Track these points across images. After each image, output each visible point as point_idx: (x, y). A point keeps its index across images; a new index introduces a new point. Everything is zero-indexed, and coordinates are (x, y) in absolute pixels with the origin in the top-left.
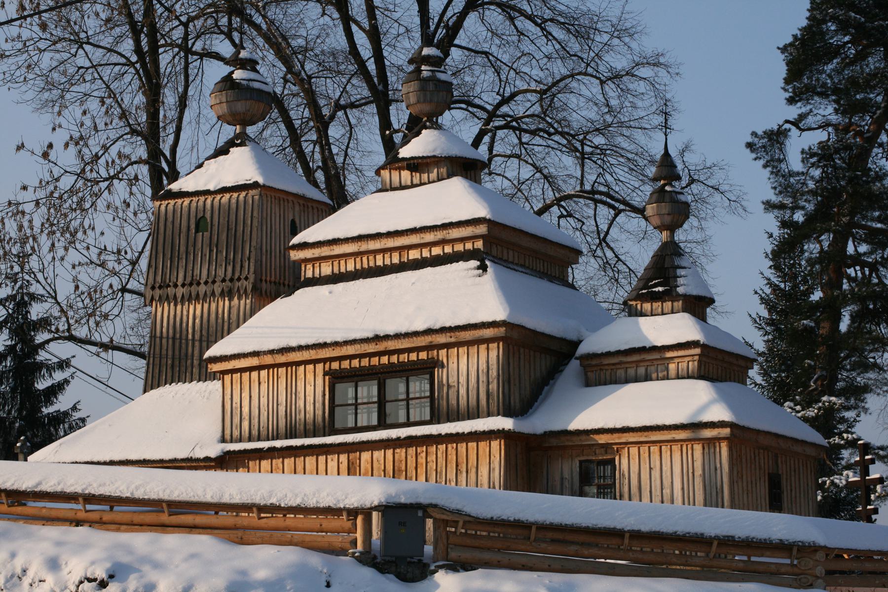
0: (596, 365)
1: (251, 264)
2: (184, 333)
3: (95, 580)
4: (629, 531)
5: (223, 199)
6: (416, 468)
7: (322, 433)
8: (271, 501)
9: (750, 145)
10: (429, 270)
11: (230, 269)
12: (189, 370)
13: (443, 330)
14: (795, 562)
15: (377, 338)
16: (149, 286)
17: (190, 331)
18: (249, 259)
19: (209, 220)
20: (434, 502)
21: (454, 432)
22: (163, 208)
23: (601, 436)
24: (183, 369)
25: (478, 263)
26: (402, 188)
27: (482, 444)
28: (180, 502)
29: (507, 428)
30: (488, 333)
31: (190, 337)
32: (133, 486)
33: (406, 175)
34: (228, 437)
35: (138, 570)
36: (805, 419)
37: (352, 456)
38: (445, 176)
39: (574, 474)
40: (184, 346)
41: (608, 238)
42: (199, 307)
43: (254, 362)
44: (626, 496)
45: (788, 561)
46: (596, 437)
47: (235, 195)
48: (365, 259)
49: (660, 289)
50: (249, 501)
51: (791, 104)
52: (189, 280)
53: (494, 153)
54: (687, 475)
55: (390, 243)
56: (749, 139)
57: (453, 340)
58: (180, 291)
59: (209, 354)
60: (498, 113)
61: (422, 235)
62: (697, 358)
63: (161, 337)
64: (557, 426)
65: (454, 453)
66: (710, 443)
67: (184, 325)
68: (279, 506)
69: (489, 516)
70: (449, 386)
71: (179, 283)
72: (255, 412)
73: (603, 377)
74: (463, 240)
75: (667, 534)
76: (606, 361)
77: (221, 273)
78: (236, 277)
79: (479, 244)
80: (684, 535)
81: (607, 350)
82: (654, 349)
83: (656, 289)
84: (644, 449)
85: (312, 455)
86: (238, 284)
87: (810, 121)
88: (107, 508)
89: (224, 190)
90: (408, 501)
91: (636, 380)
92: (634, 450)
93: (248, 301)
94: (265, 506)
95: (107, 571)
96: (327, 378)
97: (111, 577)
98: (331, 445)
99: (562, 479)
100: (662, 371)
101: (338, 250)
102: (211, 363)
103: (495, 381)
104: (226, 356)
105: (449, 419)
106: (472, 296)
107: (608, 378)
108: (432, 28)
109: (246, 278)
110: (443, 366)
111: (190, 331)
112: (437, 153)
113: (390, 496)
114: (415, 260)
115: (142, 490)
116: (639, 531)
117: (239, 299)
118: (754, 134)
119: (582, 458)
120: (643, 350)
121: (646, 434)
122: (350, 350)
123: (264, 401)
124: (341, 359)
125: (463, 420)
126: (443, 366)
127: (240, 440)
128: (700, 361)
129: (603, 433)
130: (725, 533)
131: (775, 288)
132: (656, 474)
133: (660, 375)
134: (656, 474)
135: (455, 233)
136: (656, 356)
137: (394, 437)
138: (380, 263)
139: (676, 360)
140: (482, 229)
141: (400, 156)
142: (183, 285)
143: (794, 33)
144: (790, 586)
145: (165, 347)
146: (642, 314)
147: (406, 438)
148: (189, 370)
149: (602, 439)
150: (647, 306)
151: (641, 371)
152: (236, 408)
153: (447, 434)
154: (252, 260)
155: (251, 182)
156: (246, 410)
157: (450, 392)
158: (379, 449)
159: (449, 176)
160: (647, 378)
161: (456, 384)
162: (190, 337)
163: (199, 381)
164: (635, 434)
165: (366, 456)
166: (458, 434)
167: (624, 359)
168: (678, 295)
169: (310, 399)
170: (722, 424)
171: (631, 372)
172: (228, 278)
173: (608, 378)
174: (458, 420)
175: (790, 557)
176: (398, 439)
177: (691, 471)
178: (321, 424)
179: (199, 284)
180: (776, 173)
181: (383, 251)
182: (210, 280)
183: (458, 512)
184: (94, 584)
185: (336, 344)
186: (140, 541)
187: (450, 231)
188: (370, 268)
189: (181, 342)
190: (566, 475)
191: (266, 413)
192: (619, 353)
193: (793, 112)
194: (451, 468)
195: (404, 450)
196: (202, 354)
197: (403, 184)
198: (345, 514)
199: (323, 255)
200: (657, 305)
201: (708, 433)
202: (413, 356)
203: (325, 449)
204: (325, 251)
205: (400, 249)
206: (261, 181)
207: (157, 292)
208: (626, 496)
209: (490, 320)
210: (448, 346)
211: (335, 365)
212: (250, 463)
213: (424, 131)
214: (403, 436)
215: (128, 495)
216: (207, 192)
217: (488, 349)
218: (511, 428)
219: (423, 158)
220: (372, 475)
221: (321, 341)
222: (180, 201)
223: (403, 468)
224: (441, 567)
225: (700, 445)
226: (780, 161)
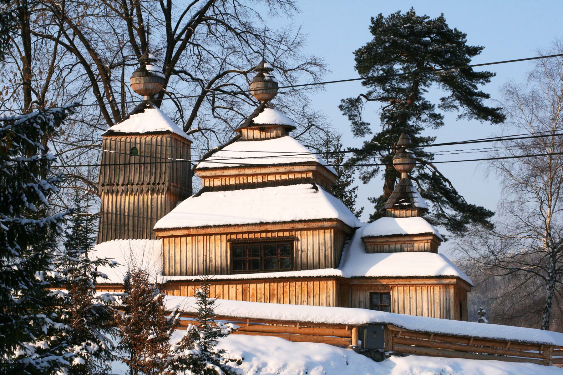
0: (373, 242)
1: (166, 176)
2: (123, 211)
3: (235, 360)
4: (474, 337)
5: (147, 138)
6: (283, 294)
7: (226, 272)
8: (308, 320)
9: (341, 107)
10: (282, 187)
11: (153, 178)
12: (126, 232)
13: (301, 221)
14: (542, 352)
15: (262, 224)
16: (101, 184)
17: (126, 210)
18: (165, 173)
19: (138, 149)
20: (391, 322)
21: (308, 276)
22: (108, 141)
23: (384, 280)
24: (122, 232)
25: (312, 186)
26: (256, 140)
27: (322, 283)
28: (257, 319)
29: (338, 275)
30: (326, 224)
31: (126, 214)
32: (231, 310)
33: (257, 134)
34: (167, 272)
35: (255, 356)
37: (244, 286)
38: (280, 135)
39: (367, 299)
40: (123, 219)
42: (132, 198)
43: (186, 232)
44: (396, 311)
45: (538, 352)
46: (381, 281)
47: (155, 137)
48: (241, 178)
49: (406, 204)
50: (296, 319)
51: (365, 85)
52: (126, 182)
53: (215, 106)
54: (431, 302)
55: (258, 171)
56: (340, 103)
57: (306, 227)
58: (121, 188)
59: (156, 227)
60: (180, 74)
61: (277, 168)
62: (430, 241)
63: (108, 213)
64: (359, 274)
65: (306, 286)
66: (446, 286)
67: (123, 207)
68: (313, 323)
69: (414, 329)
70: (302, 251)
71: (120, 184)
72: (184, 260)
73: (376, 248)
74: (300, 172)
75: (490, 339)
76: (379, 240)
77: (147, 179)
78: (157, 182)
79: (310, 175)
80: (497, 339)
81: (380, 234)
82: (407, 235)
83: (404, 204)
84: (407, 288)
85: (220, 284)
86: (158, 187)
87: (374, 95)
89: (148, 133)
90: (380, 322)
91: (395, 251)
92: (401, 288)
93: (163, 196)
94: (305, 322)
95: (241, 355)
96: (229, 243)
97: (243, 359)
98: (234, 280)
99: (360, 301)
100: (410, 247)
101: (226, 173)
103: (329, 250)
104: (169, 229)
105: (302, 269)
106: (312, 204)
107: (379, 249)
108: (173, 29)
109: (163, 184)
110: (298, 240)
111: (126, 210)
112: (277, 122)
113: (371, 319)
114: (272, 181)
115: (236, 312)
116: (478, 337)
117: (158, 195)
118: (343, 101)
119: (371, 291)
120: (401, 235)
121: (409, 280)
122: (245, 229)
123: (189, 254)
124: (237, 233)
125: (311, 269)
126: (298, 240)
127: (175, 274)
128: (431, 244)
130: (514, 339)
132: (413, 301)
133: (409, 249)
134: (413, 301)
135: (297, 168)
136: (408, 239)
137: (272, 277)
138: (255, 181)
139: (418, 242)
140: (313, 168)
141: (256, 122)
142: (123, 185)
144: (539, 364)
145: (110, 219)
146: (395, 216)
147: (279, 278)
148: (126, 232)
149: (384, 282)
150: (397, 212)
151: (398, 246)
152: (172, 257)
153: (304, 277)
154: (167, 174)
155: (165, 130)
156: (178, 258)
157: (303, 254)
158: (261, 283)
159: (283, 136)
160: (401, 250)
161: (306, 250)
162: (126, 214)
163: (133, 239)
164: (403, 280)
165: (253, 286)
166: (310, 277)
167: (389, 240)
168: (416, 207)
169: (218, 254)
170: (452, 277)
171: (392, 246)
172: (152, 183)
173: (379, 249)
174: (308, 269)
175: (539, 350)
176: (275, 278)
177: (432, 300)
178: (225, 268)
179: (132, 184)
180: (355, 123)
181: (253, 175)
182: (140, 183)
183: (401, 327)
184: (235, 363)
185: (237, 225)
186: (259, 341)
187: (294, 167)
188: (244, 183)
189: (120, 217)
190: (362, 299)
191: (191, 261)
192: (387, 236)
193: (365, 90)
194: (304, 294)
195: (276, 284)
196: (152, 225)
197: (255, 137)
198: (298, 324)
199: (217, 174)
200: (403, 212)
201: (447, 281)
202: (281, 234)
203: (243, 282)
204: (218, 173)
205: (263, 175)
206: (171, 130)
207: (107, 188)
208: (396, 311)
209: (329, 218)
210: (301, 230)
211: (233, 237)
212: (182, 287)
213: (265, 109)
214: (278, 277)
215: (228, 314)
216: (138, 134)
217: (325, 232)
219: (269, 124)
221: (228, 223)
222: (119, 137)
223: (276, 293)
224: (392, 354)
225: (438, 287)
226: (356, 116)
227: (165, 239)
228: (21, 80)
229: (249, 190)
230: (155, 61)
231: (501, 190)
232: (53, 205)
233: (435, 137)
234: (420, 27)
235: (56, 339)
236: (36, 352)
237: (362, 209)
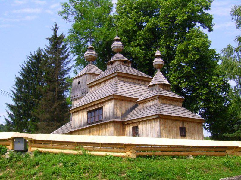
228: (153, 172)
229: (104, 143)
233: (47, 39)
234: (226, 105)
235: (16, 105)
237: (30, 53)
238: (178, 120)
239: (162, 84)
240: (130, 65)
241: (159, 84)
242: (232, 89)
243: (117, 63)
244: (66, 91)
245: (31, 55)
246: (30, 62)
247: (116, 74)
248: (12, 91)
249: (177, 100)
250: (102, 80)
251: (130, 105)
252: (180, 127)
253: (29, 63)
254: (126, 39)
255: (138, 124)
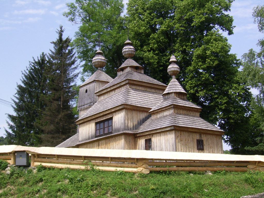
36: (231, 33)
41: (100, 130)
88: (102, 162)
102: (62, 40)
129: (90, 120)
131: (166, 135)
143: (70, 38)
209: (169, 159)
218: (15, 116)
220: (163, 151)
227: (99, 134)
230: (112, 30)
231: (5, 127)
232: (166, 28)
233: (51, 43)
236: (112, 132)
237: (33, 58)
238: (195, 132)
239: (182, 126)
240: (143, 72)
241: (174, 93)
242: (255, 98)
243: (128, 69)
244: (72, 100)
245: (34, 60)
246: (33, 68)
247: (127, 82)
248: (13, 100)
249: (194, 110)
250: (112, 88)
251: (142, 116)
252: (197, 140)
253: (32, 69)
254: (138, 43)
255: (151, 136)
